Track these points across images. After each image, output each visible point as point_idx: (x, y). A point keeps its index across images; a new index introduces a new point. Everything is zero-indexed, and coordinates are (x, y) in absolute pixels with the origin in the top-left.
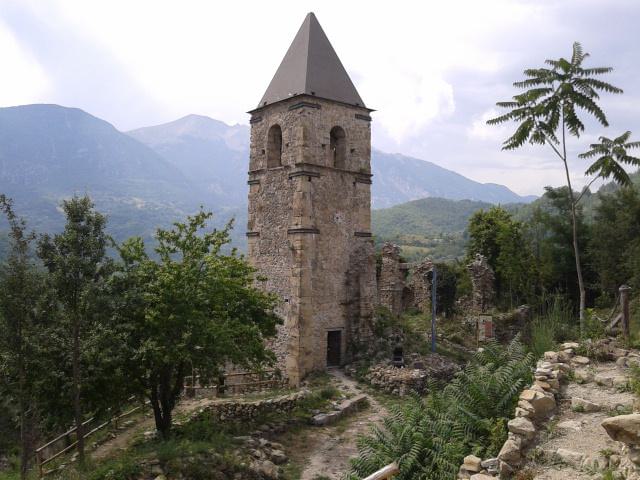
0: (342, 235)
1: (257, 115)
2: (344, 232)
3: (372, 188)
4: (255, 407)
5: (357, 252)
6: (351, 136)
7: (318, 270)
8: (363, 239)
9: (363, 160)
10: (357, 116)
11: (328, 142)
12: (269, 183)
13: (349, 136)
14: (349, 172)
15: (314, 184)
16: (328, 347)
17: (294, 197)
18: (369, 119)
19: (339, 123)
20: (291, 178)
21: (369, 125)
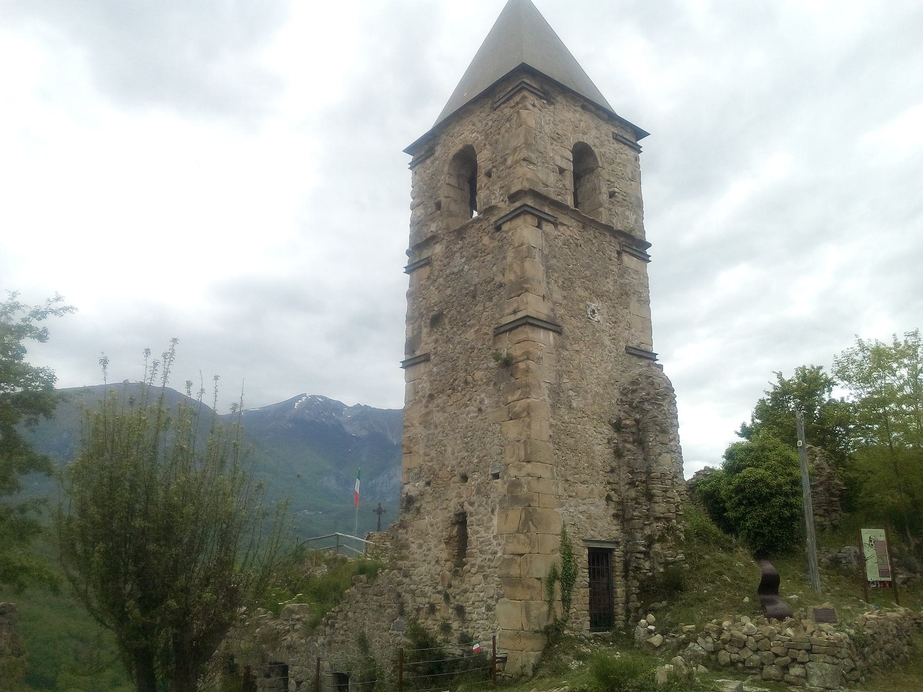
0: (603, 346)
3: (651, 268)
5: (633, 383)
7: (563, 410)
9: (633, 217)
11: (569, 167)
14: (609, 228)
15: (546, 234)
16: (590, 585)
17: (509, 259)
18: (638, 149)
19: (589, 140)
20: (498, 228)
21: (637, 159)
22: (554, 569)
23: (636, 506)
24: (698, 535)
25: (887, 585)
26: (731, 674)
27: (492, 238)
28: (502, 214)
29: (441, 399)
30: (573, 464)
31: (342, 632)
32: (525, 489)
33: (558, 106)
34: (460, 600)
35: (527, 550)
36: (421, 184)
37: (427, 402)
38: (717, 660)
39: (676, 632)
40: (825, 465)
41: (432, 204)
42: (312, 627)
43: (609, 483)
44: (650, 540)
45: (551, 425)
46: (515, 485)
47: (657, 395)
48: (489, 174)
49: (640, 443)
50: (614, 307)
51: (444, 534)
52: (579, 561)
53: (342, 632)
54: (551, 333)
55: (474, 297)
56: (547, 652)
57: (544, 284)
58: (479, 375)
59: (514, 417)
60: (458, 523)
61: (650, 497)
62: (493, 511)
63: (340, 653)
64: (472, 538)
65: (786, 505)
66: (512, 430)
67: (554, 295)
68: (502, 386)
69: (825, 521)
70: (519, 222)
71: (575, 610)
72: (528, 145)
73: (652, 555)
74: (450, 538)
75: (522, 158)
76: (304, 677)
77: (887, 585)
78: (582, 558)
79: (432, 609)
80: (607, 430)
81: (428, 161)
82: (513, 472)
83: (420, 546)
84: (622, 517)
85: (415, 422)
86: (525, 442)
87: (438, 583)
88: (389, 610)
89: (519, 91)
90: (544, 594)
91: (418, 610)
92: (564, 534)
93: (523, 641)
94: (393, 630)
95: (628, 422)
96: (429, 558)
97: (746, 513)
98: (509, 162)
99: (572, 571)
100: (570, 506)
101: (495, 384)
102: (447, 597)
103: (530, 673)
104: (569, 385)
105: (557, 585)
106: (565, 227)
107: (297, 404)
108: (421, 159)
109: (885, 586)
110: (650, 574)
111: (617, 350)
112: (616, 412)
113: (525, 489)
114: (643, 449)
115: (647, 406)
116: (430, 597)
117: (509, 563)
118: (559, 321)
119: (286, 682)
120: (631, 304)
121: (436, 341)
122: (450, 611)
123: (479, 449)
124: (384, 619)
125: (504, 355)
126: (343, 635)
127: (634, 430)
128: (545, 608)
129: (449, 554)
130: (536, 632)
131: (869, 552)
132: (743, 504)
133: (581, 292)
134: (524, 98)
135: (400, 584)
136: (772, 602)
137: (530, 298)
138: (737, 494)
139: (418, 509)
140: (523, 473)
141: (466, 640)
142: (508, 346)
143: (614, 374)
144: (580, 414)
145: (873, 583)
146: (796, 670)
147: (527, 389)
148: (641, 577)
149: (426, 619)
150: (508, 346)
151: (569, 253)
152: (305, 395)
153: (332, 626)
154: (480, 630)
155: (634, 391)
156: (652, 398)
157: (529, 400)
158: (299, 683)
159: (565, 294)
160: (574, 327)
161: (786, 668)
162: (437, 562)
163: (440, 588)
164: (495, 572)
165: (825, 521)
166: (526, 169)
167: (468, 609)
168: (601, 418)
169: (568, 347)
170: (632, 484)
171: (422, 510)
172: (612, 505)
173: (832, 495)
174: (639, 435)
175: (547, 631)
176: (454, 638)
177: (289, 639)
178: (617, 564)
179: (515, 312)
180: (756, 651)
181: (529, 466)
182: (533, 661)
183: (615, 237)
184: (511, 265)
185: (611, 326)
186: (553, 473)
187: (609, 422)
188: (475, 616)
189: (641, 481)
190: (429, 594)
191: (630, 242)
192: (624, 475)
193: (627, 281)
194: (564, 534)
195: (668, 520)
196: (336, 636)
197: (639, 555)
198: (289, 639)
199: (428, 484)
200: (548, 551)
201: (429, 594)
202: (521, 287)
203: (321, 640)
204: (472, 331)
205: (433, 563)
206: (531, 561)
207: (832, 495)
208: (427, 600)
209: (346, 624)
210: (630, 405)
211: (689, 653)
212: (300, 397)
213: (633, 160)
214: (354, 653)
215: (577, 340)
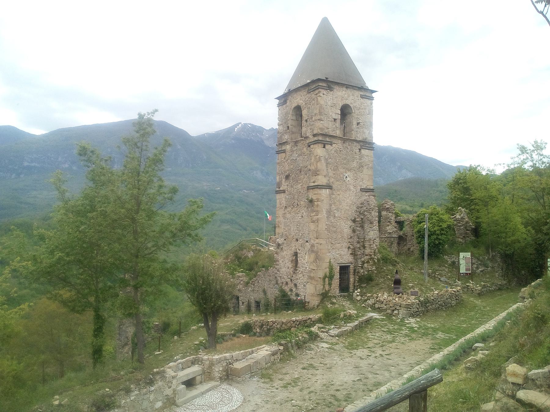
0: (350, 190)
1: (283, 100)
2: (352, 188)
4: (283, 323)
5: (361, 204)
6: (357, 112)
7: (332, 218)
8: (367, 194)
9: (367, 132)
10: (362, 97)
12: (292, 151)
13: (355, 113)
14: (356, 141)
16: (340, 278)
17: (312, 160)
19: (348, 102)
20: (309, 146)
22: (326, 274)
23: (359, 250)
24: (383, 259)
25: (468, 274)
26: (378, 311)
27: (307, 149)
28: (311, 141)
29: (289, 209)
30: (335, 237)
31: (257, 287)
32: (316, 248)
33: (335, 90)
34: (295, 282)
35: (316, 269)
36: (282, 115)
37: (284, 209)
38: (375, 306)
39: (365, 296)
40: (466, 217)
41: (286, 126)
42: (247, 284)
43: (349, 242)
44: (363, 263)
45: (327, 225)
46: (313, 246)
47: (370, 209)
48: (306, 121)
49: (362, 227)
50: (356, 173)
51: (290, 259)
52: (336, 271)
53: (257, 287)
54: (328, 189)
55: (301, 172)
56: (322, 301)
57: (325, 171)
58: (302, 203)
59: (313, 222)
60: (295, 255)
61: (364, 247)
62: (306, 254)
63: (257, 294)
64: (299, 261)
65: (437, 238)
66: (312, 226)
67: (330, 174)
68: (309, 209)
69: (463, 241)
70: (316, 146)
71: (333, 287)
72: (320, 114)
73: (364, 268)
74: (292, 260)
75: (318, 119)
76: (245, 301)
77: (468, 274)
78: (337, 270)
79: (287, 283)
80: (350, 223)
81: (284, 106)
82: (312, 241)
83: (283, 262)
84: (354, 254)
85: (280, 216)
86: (316, 232)
87: (289, 275)
88: (273, 282)
89: (318, 89)
90: (322, 283)
91: (282, 283)
92: (330, 262)
93: (314, 297)
94: (274, 289)
95: (358, 219)
96: (286, 266)
97: (421, 241)
98: (313, 119)
99: (333, 274)
100: (333, 252)
101: (307, 208)
102: (291, 280)
103: (316, 307)
104: (334, 209)
105: (327, 279)
106: (336, 144)
107: (236, 129)
108: (281, 104)
109: (467, 275)
110: (363, 274)
111: (356, 191)
112: (354, 215)
113: (316, 248)
114: (363, 229)
115: (366, 213)
116: (286, 279)
117: (310, 272)
118: (331, 184)
119: (239, 302)
120: (364, 171)
121: (288, 185)
122: (292, 285)
123: (302, 231)
124: (271, 285)
125: (310, 199)
126: (257, 288)
127: (360, 222)
128: (322, 287)
129: (292, 266)
130: (318, 295)
131: (462, 262)
132: (420, 237)
133: (342, 170)
134: (319, 92)
135: (276, 273)
136: (399, 288)
137: (319, 177)
138: (418, 233)
139: (282, 249)
140: (315, 242)
141: (297, 295)
142: (312, 195)
143: (354, 201)
144: (339, 219)
145: (462, 274)
146: (396, 312)
147: (317, 212)
148: (360, 275)
149: (285, 286)
150: (312, 195)
151: (337, 155)
152: (240, 123)
153: (254, 285)
154: (302, 292)
155: (361, 207)
156: (368, 210)
157: (318, 217)
158: (243, 303)
159: (334, 172)
160: (338, 185)
161: (393, 311)
162: (288, 268)
163: (289, 277)
164: (306, 274)
165: (463, 241)
166: (319, 124)
167: (298, 285)
168: (348, 218)
169: (335, 194)
170: (358, 242)
171: (283, 249)
172: (350, 250)
173: (467, 230)
174: (362, 224)
175: (322, 294)
176: (294, 294)
177: (239, 287)
178: (351, 271)
179: (314, 182)
180: (386, 305)
181: (317, 240)
182: (317, 304)
183: (358, 143)
184: (313, 163)
185: (354, 181)
186: (326, 241)
187: (351, 220)
188: (300, 287)
189: (362, 241)
190: (286, 278)
191: (365, 143)
192: (356, 239)
193: (363, 161)
194: (330, 262)
195: (370, 255)
196: (256, 288)
197: (359, 268)
198: (239, 287)
199: (285, 240)
200: (324, 269)
201: (286, 278)
202: (316, 173)
203: (250, 289)
204: (300, 185)
205: (287, 268)
206: (317, 272)
207: (467, 230)
208: (285, 280)
209: (259, 285)
210: (360, 213)
211: (367, 303)
212: (238, 125)
213: (370, 104)
214: (262, 295)
215: (338, 190)
